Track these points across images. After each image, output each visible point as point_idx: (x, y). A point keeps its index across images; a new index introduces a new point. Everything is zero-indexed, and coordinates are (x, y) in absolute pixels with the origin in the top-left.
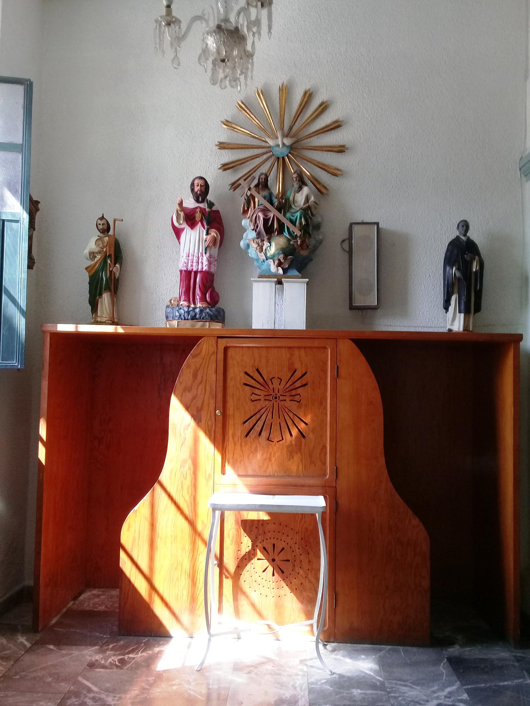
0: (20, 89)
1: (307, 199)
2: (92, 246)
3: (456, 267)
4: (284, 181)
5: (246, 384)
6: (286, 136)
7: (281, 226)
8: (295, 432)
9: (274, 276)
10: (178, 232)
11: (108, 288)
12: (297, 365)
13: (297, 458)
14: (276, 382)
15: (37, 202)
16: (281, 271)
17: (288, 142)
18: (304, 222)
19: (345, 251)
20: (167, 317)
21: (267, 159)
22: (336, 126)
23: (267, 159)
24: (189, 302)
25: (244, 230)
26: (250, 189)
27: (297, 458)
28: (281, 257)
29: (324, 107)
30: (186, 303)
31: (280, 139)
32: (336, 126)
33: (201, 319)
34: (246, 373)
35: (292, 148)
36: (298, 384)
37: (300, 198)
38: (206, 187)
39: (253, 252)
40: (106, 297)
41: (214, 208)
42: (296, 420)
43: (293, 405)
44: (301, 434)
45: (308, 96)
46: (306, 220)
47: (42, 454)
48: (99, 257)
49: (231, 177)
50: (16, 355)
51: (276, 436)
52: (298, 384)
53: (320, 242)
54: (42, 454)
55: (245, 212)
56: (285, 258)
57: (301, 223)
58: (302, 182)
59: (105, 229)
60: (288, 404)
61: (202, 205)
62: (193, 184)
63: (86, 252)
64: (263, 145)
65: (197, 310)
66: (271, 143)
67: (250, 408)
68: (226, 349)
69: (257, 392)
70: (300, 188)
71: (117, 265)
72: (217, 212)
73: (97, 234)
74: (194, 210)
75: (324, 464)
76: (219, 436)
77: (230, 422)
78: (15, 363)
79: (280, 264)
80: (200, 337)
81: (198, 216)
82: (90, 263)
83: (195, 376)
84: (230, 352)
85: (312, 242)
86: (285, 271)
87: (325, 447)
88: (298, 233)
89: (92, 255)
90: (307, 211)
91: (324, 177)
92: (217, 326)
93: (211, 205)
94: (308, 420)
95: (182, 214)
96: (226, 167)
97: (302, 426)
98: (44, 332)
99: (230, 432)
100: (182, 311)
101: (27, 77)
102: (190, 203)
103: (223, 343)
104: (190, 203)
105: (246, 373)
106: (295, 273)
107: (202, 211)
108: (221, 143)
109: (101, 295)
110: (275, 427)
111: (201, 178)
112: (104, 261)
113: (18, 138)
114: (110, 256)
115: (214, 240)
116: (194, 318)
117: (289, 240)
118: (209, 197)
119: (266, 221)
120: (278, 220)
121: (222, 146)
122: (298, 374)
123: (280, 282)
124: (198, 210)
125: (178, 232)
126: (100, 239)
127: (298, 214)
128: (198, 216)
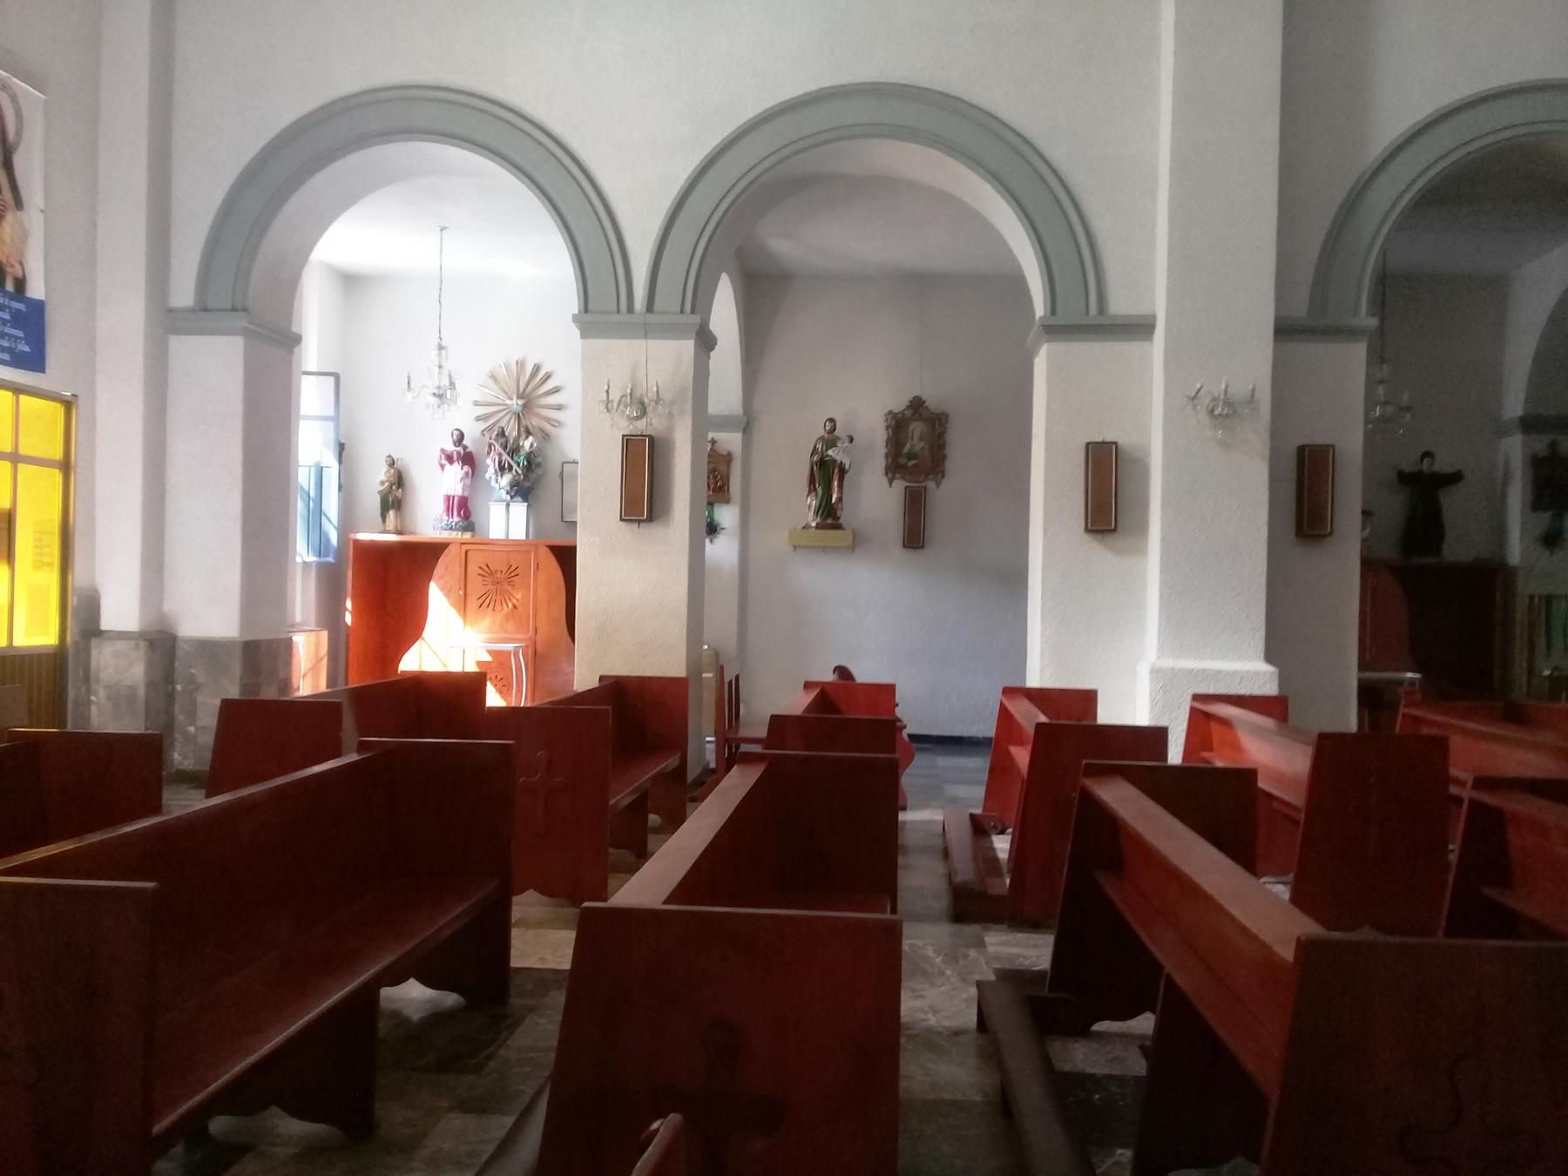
0: (331, 380)
1: (532, 445)
2: (382, 477)
3: (333, 546)
4: (978, 163)
5: (479, 574)
6: (520, 397)
7: (510, 468)
8: (510, 605)
9: (504, 501)
10: (442, 467)
11: (393, 507)
12: (512, 562)
13: (511, 622)
14: (499, 573)
15: (343, 444)
16: (509, 498)
17: (520, 402)
18: (525, 463)
19: (300, 555)
20: (434, 528)
21: (507, 414)
22: (556, 390)
23: (507, 414)
24: (448, 515)
25: (488, 466)
26: (490, 438)
27: (511, 622)
28: (508, 488)
29: (548, 377)
30: (447, 518)
31: (515, 400)
32: (556, 390)
33: (455, 530)
34: (480, 568)
35: (525, 406)
36: (513, 574)
37: (527, 444)
38: (461, 436)
39: (493, 483)
40: (392, 513)
41: (468, 450)
42: (511, 598)
43: (509, 588)
44: (514, 606)
45: (537, 368)
46: (528, 462)
47: (348, 619)
48: (387, 484)
49: (483, 425)
50: (332, 555)
51: (498, 608)
52: (513, 574)
53: (541, 476)
54: (348, 619)
55: (489, 453)
56: (511, 488)
57: (523, 464)
58: (528, 433)
59: (392, 463)
60: (506, 587)
61: (458, 449)
62: (452, 434)
63: (378, 480)
64: (488, 412)
65: (454, 524)
66: (508, 402)
67: (483, 590)
68: (467, 552)
69: (486, 579)
70: (527, 437)
71: (400, 490)
72: (470, 453)
73: (384, 468)
74: (452, 452)
75: (529, 625)
76: (462, 607)
77: (469, 598)
78: (331, 559)
79: (508, 493)
80: (450, 544)
81: (455, 458)
82: (382, 488)
83: (446, 569)
84: (469, 553)
85: (533, 476)
86: (512, 497)
87: (529, 614)
88: (520, 472)
89: (382, 483)
90: (530, 457)
91: (548, 427)
92: (467, 536)
93: (465, 448)
94: (519, 596)
95: (443, 456)
96: (478, 419)
97: (515, 601)
98: (349, 540)
99: (469, 605)
100: (443, 524)
101: (336, 371)
102: (450, 447)
103: (465, 547)
104: (450, 447)
105: (480, 568)
106: (519, 499)
107: (458, 453)
108: (475, 401)
109: (388, 511)
110: (498, 602)
111: (458, 430)
112: (391, 487)
113: (331, 412)
114: (394, 484)
115: (467, 474)
116: (451, 529)
117: (515, 476)
118: (464, 442)
119: (500, 462)
120: (509, 464)
121: (476, 404)
122: (512, 568)
123: (508, 505)
124: (455, 453)
125: (442, 467)
126: (388, 471)
127: (522, 458)
128: (455, 458)
